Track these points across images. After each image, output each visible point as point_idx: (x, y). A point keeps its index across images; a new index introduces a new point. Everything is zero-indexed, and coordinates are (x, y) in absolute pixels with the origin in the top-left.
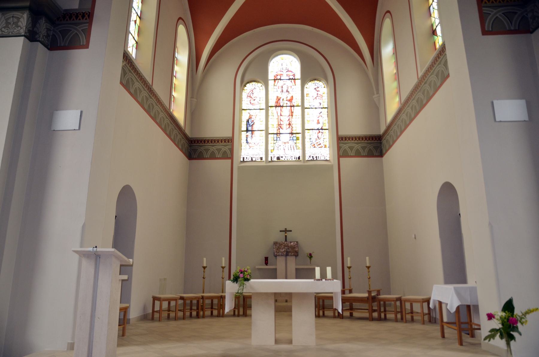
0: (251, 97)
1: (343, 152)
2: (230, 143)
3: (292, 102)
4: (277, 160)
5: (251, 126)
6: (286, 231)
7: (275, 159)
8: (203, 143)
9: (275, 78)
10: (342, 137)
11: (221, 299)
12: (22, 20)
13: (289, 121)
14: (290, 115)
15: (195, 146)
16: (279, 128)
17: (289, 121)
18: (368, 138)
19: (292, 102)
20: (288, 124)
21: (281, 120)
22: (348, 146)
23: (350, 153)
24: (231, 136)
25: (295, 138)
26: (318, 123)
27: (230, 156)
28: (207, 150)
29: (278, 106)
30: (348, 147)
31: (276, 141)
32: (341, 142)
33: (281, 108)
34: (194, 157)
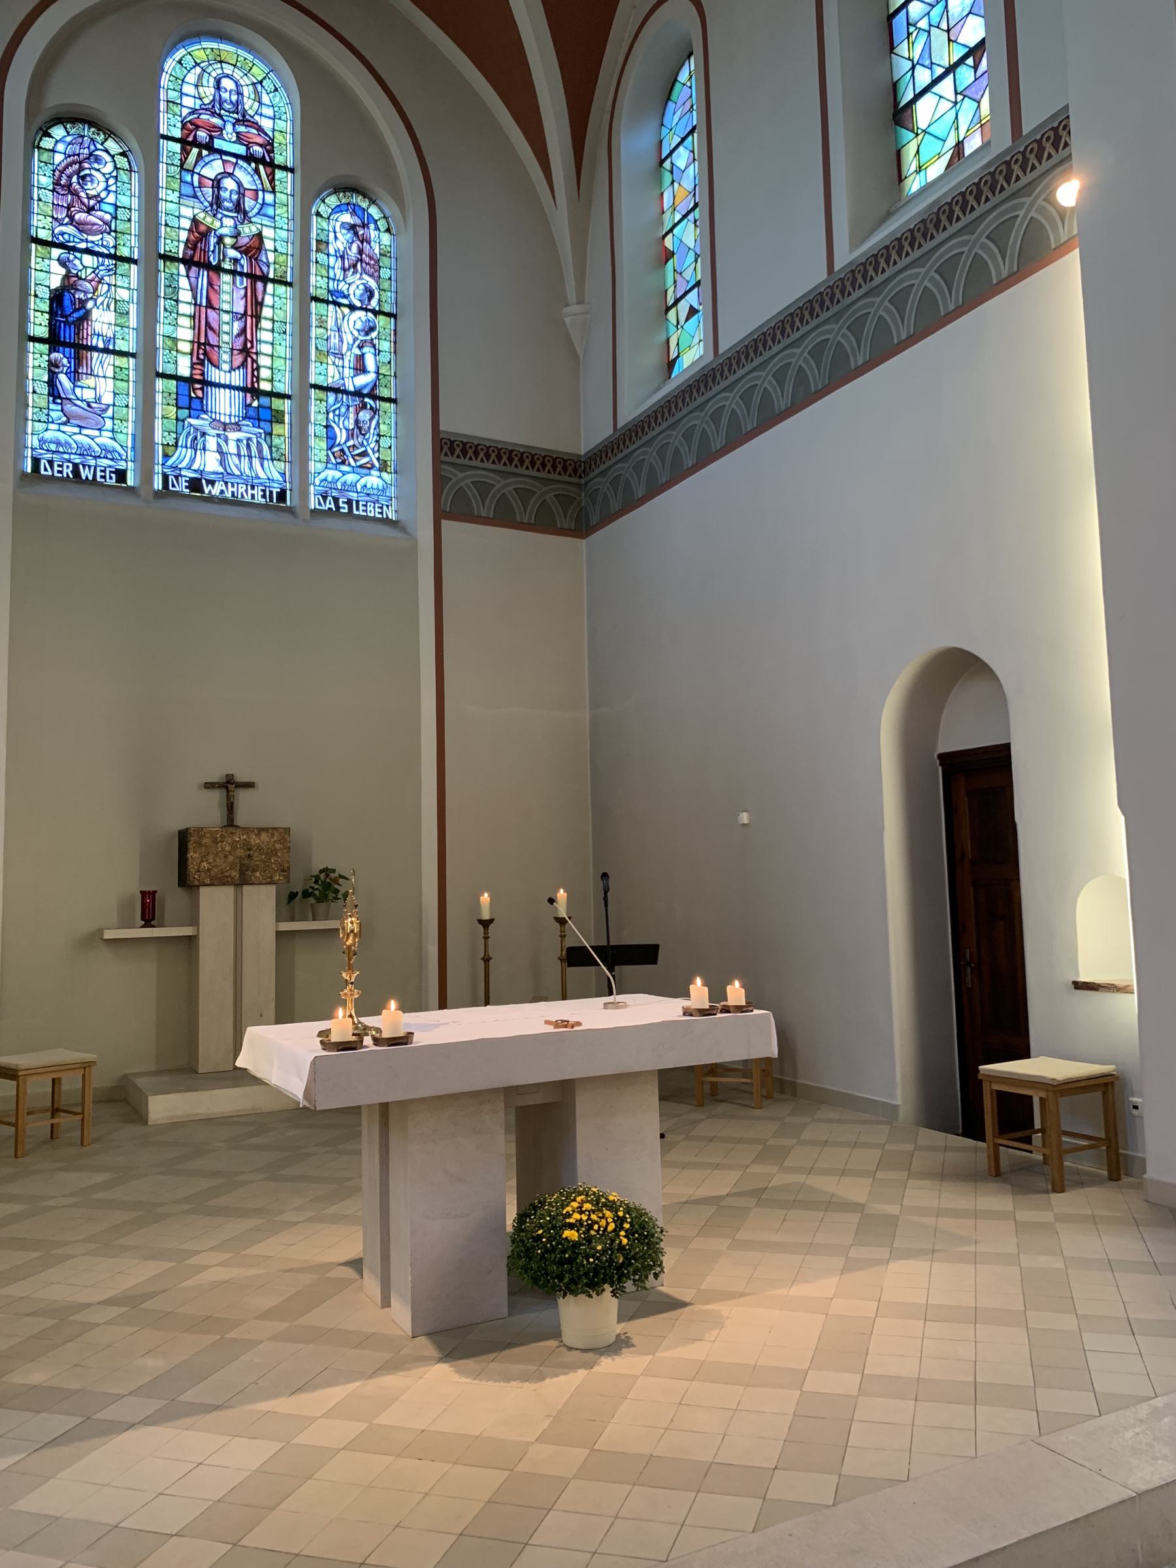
0: (75, 194)
3: (256, 259)
4: (192, 491)
5: (73, 322)
6: (229, 785)
7: (182, 487)
9: (188, 136)
10: (452, 442)
13: (242, 338)
14: (249, 313)
16: (202, 357)
17: (242, 338)
19: (256, 259)
20: (241, 351)
21: (212, 329)
22: (516, 486)
23: (478, 507)
25: (269, 412)
26: (360, 368)
29: (199, 265)
30: (472, 482)
31: (187, 411)
33: (213, 275)
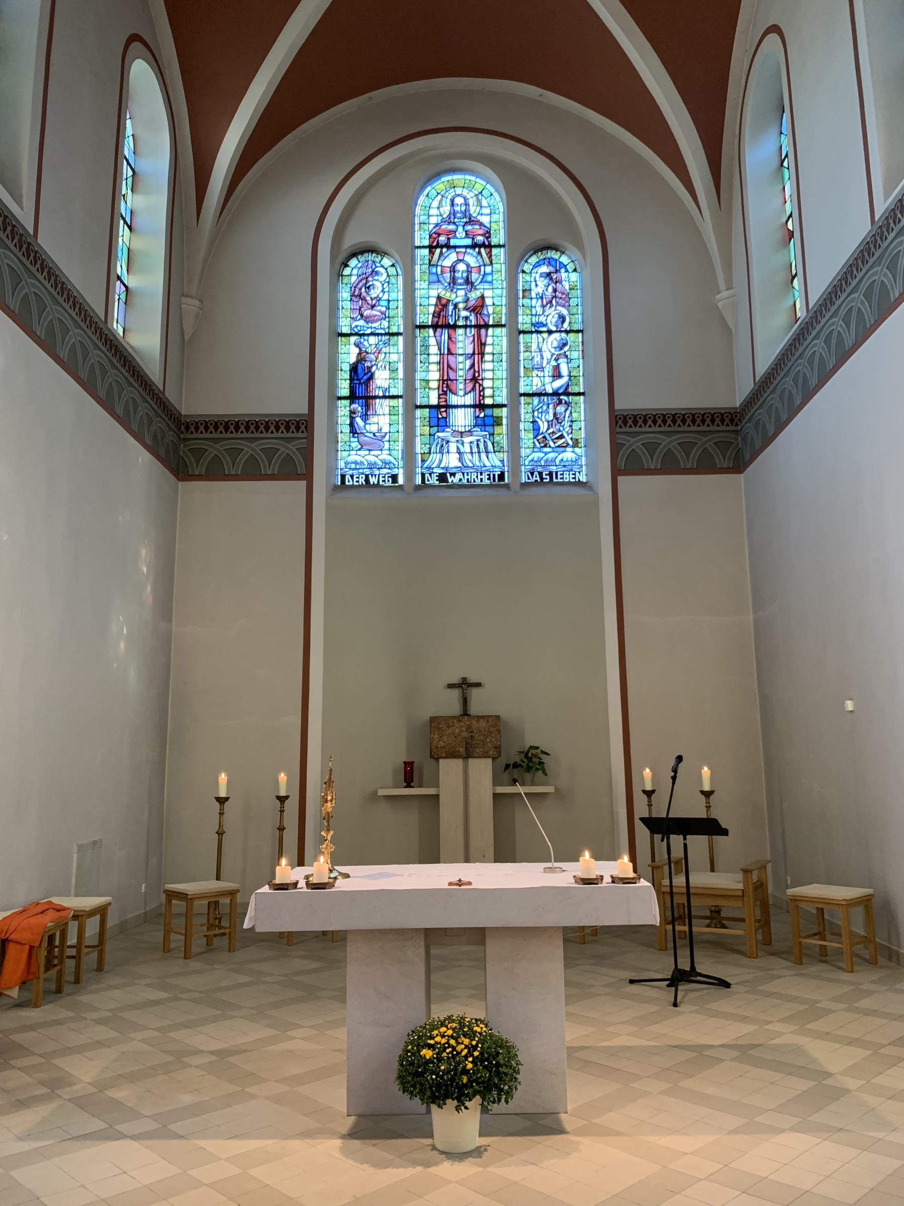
24: (305, 410)
27: (305, 472)
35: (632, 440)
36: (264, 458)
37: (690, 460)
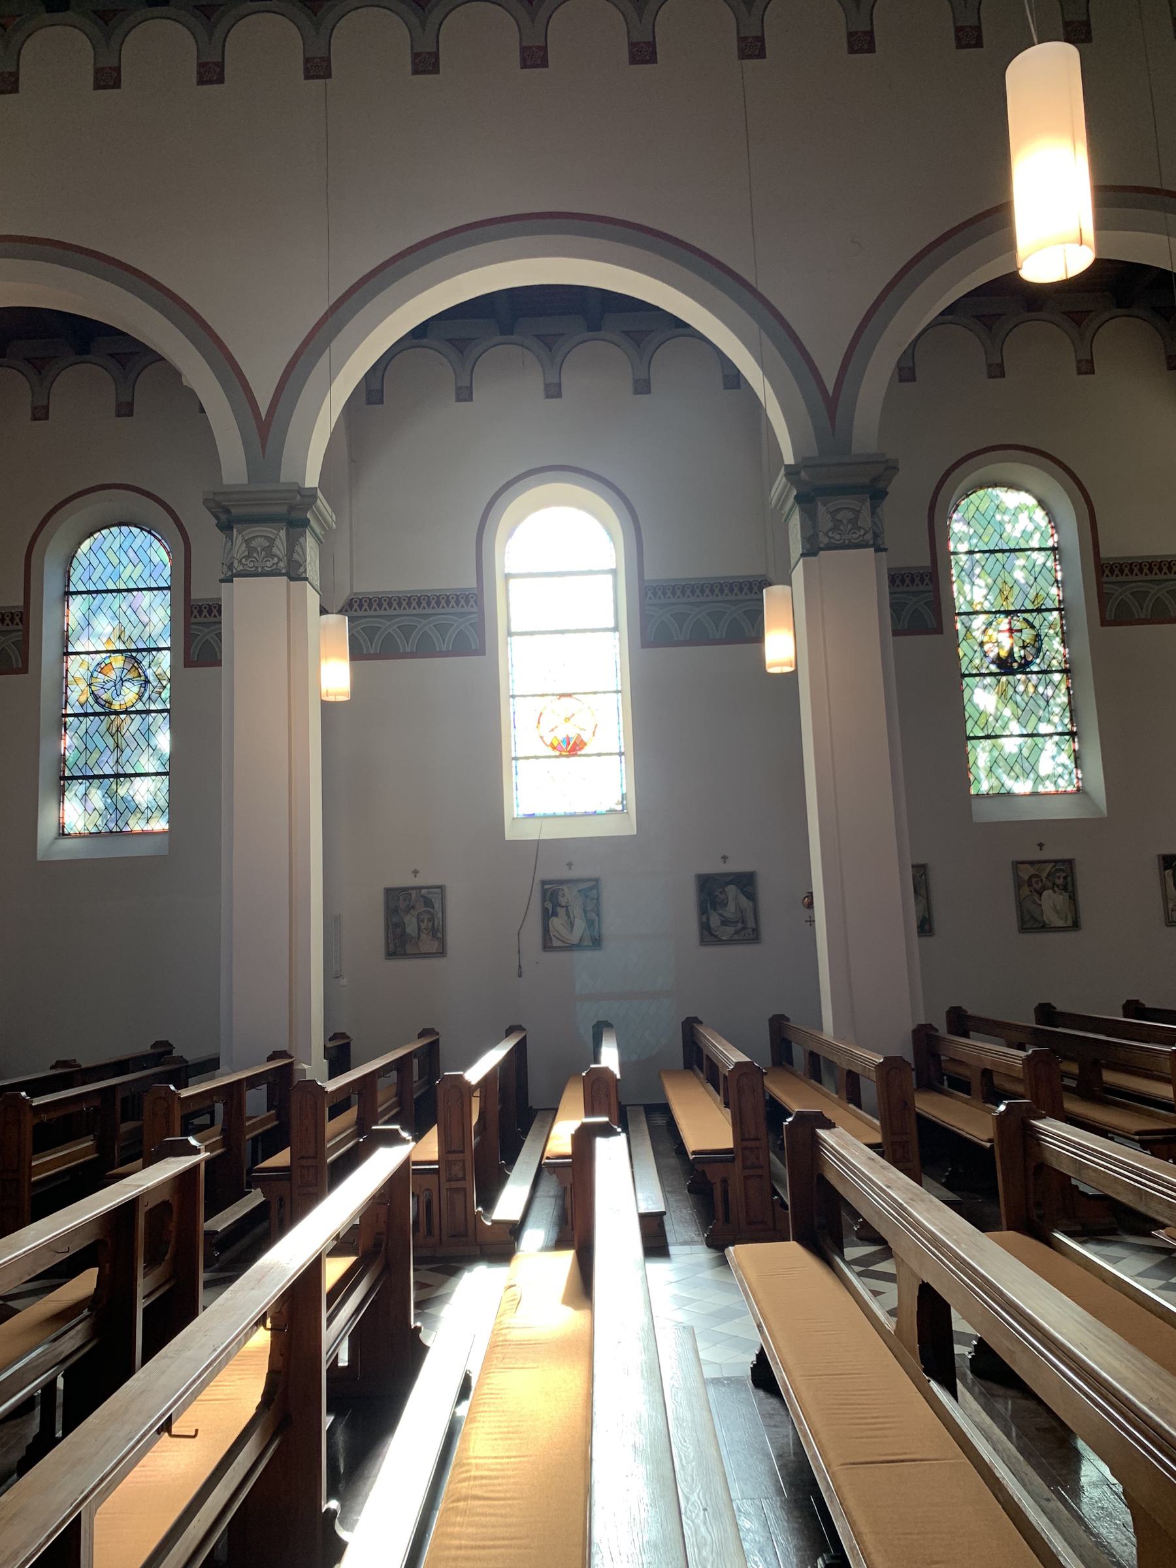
1: (1154, 604)
2: (17, 624)
8: (927, 584)
11: (1109, 1077)
12: (278, 541)
15: (450, 614)
18: (1148, 567)
22: (1167, 590)
24: (928, 563)
27: (20, 665)
28: (406, 631)
32: (1108, 580)
34: (444, 649)
35: (206, 630)
36: (378, 634)
37: (410, 645)
